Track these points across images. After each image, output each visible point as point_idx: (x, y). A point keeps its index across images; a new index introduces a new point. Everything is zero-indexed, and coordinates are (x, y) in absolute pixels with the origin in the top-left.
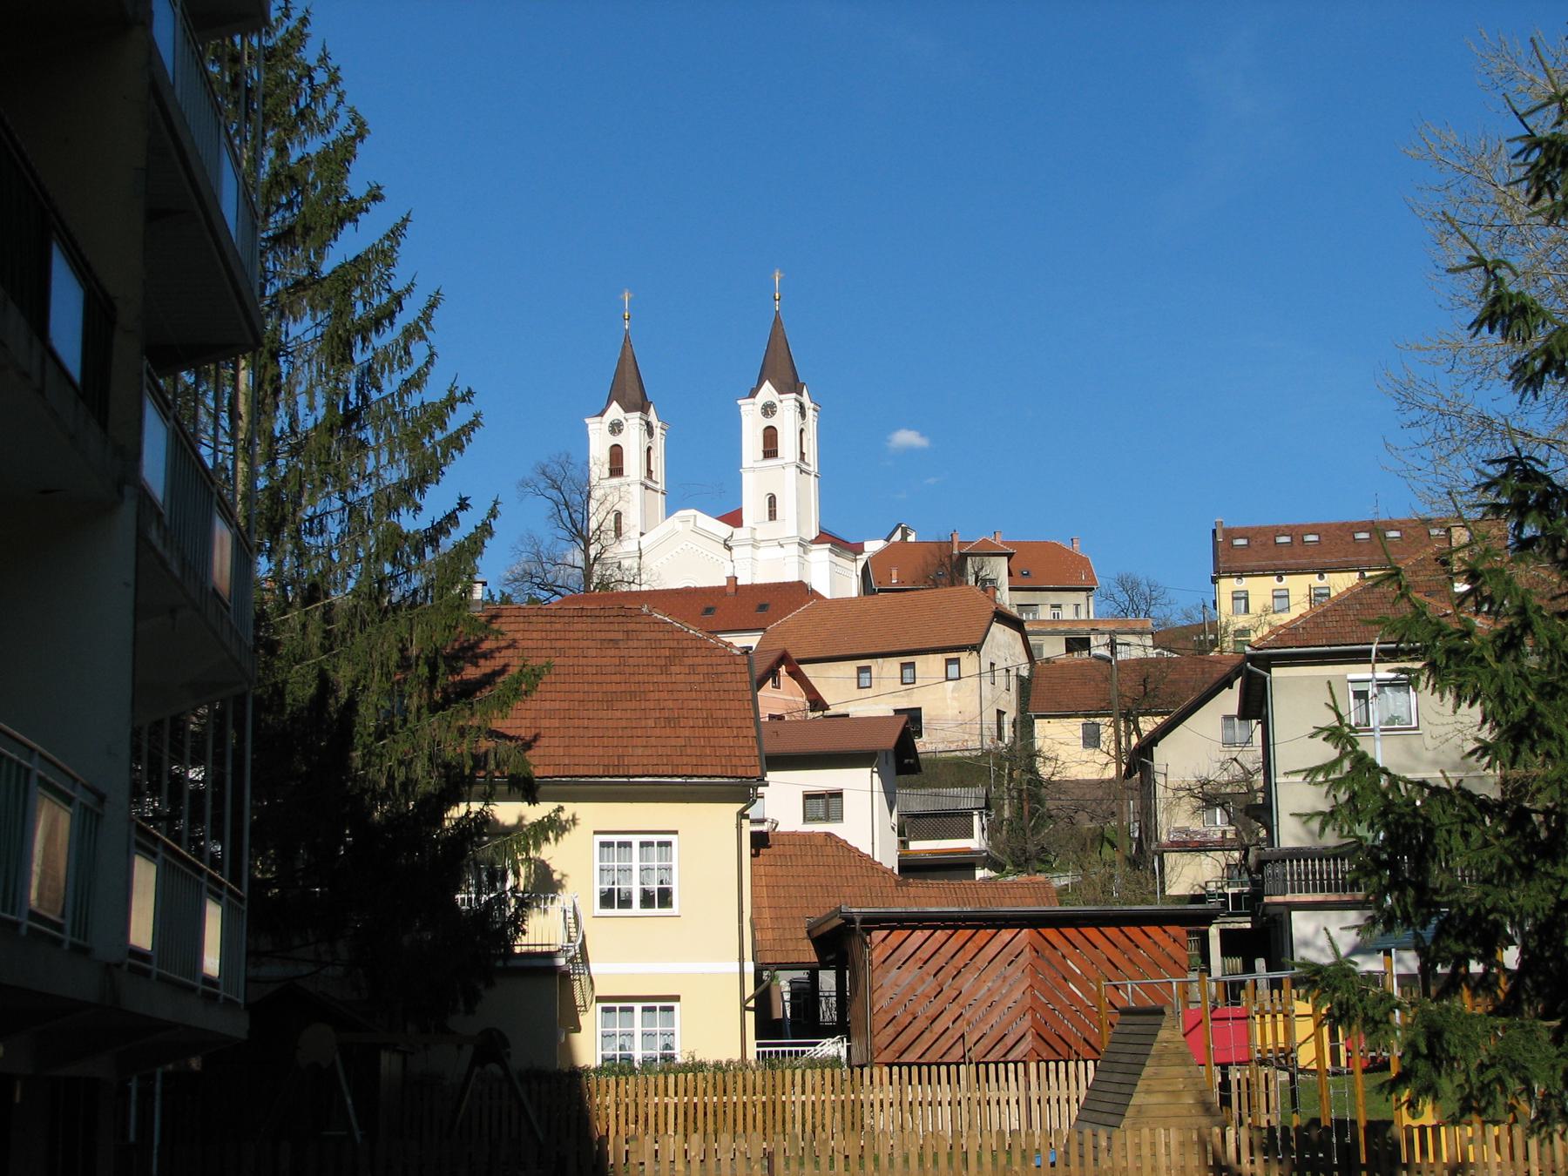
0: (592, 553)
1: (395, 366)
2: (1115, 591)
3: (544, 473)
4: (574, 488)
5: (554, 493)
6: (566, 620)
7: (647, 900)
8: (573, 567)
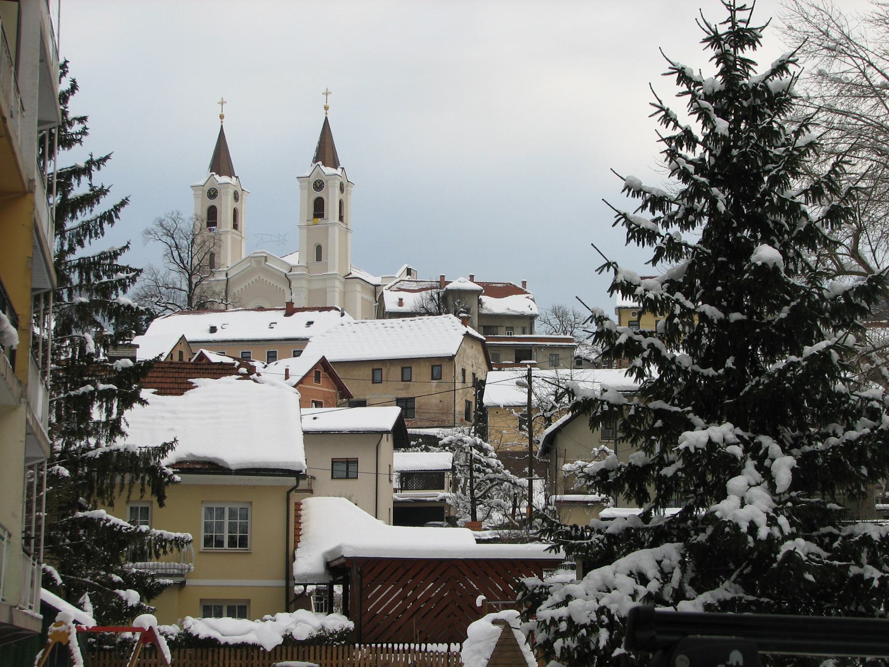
0: (194, 281)
1: (93, 235)
2: (550, 317)
3: (162, 225)
4: (182, 235)
5: (169, 240)
6: (188, 371)
7: (232, 542)
8: (180, 290)
